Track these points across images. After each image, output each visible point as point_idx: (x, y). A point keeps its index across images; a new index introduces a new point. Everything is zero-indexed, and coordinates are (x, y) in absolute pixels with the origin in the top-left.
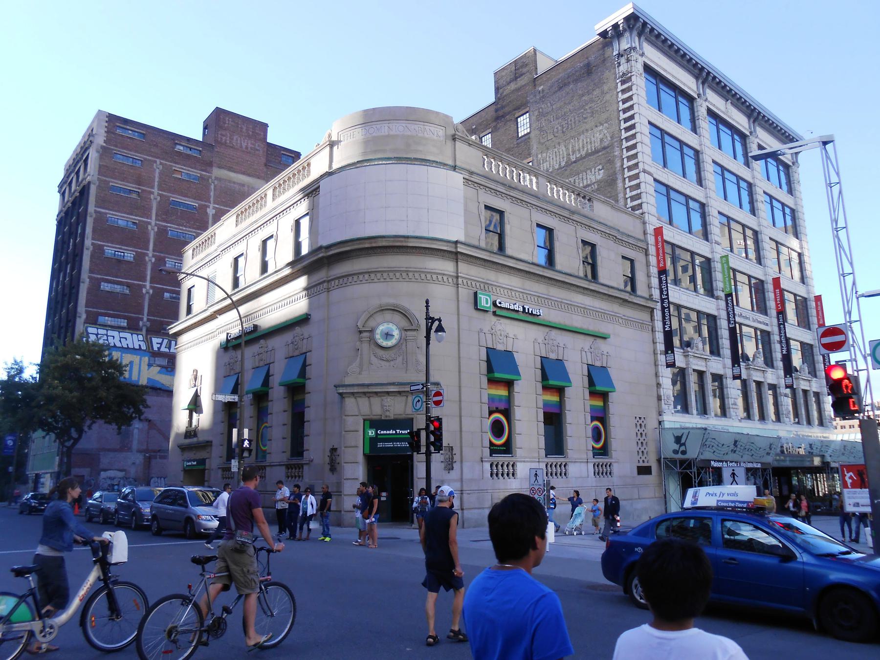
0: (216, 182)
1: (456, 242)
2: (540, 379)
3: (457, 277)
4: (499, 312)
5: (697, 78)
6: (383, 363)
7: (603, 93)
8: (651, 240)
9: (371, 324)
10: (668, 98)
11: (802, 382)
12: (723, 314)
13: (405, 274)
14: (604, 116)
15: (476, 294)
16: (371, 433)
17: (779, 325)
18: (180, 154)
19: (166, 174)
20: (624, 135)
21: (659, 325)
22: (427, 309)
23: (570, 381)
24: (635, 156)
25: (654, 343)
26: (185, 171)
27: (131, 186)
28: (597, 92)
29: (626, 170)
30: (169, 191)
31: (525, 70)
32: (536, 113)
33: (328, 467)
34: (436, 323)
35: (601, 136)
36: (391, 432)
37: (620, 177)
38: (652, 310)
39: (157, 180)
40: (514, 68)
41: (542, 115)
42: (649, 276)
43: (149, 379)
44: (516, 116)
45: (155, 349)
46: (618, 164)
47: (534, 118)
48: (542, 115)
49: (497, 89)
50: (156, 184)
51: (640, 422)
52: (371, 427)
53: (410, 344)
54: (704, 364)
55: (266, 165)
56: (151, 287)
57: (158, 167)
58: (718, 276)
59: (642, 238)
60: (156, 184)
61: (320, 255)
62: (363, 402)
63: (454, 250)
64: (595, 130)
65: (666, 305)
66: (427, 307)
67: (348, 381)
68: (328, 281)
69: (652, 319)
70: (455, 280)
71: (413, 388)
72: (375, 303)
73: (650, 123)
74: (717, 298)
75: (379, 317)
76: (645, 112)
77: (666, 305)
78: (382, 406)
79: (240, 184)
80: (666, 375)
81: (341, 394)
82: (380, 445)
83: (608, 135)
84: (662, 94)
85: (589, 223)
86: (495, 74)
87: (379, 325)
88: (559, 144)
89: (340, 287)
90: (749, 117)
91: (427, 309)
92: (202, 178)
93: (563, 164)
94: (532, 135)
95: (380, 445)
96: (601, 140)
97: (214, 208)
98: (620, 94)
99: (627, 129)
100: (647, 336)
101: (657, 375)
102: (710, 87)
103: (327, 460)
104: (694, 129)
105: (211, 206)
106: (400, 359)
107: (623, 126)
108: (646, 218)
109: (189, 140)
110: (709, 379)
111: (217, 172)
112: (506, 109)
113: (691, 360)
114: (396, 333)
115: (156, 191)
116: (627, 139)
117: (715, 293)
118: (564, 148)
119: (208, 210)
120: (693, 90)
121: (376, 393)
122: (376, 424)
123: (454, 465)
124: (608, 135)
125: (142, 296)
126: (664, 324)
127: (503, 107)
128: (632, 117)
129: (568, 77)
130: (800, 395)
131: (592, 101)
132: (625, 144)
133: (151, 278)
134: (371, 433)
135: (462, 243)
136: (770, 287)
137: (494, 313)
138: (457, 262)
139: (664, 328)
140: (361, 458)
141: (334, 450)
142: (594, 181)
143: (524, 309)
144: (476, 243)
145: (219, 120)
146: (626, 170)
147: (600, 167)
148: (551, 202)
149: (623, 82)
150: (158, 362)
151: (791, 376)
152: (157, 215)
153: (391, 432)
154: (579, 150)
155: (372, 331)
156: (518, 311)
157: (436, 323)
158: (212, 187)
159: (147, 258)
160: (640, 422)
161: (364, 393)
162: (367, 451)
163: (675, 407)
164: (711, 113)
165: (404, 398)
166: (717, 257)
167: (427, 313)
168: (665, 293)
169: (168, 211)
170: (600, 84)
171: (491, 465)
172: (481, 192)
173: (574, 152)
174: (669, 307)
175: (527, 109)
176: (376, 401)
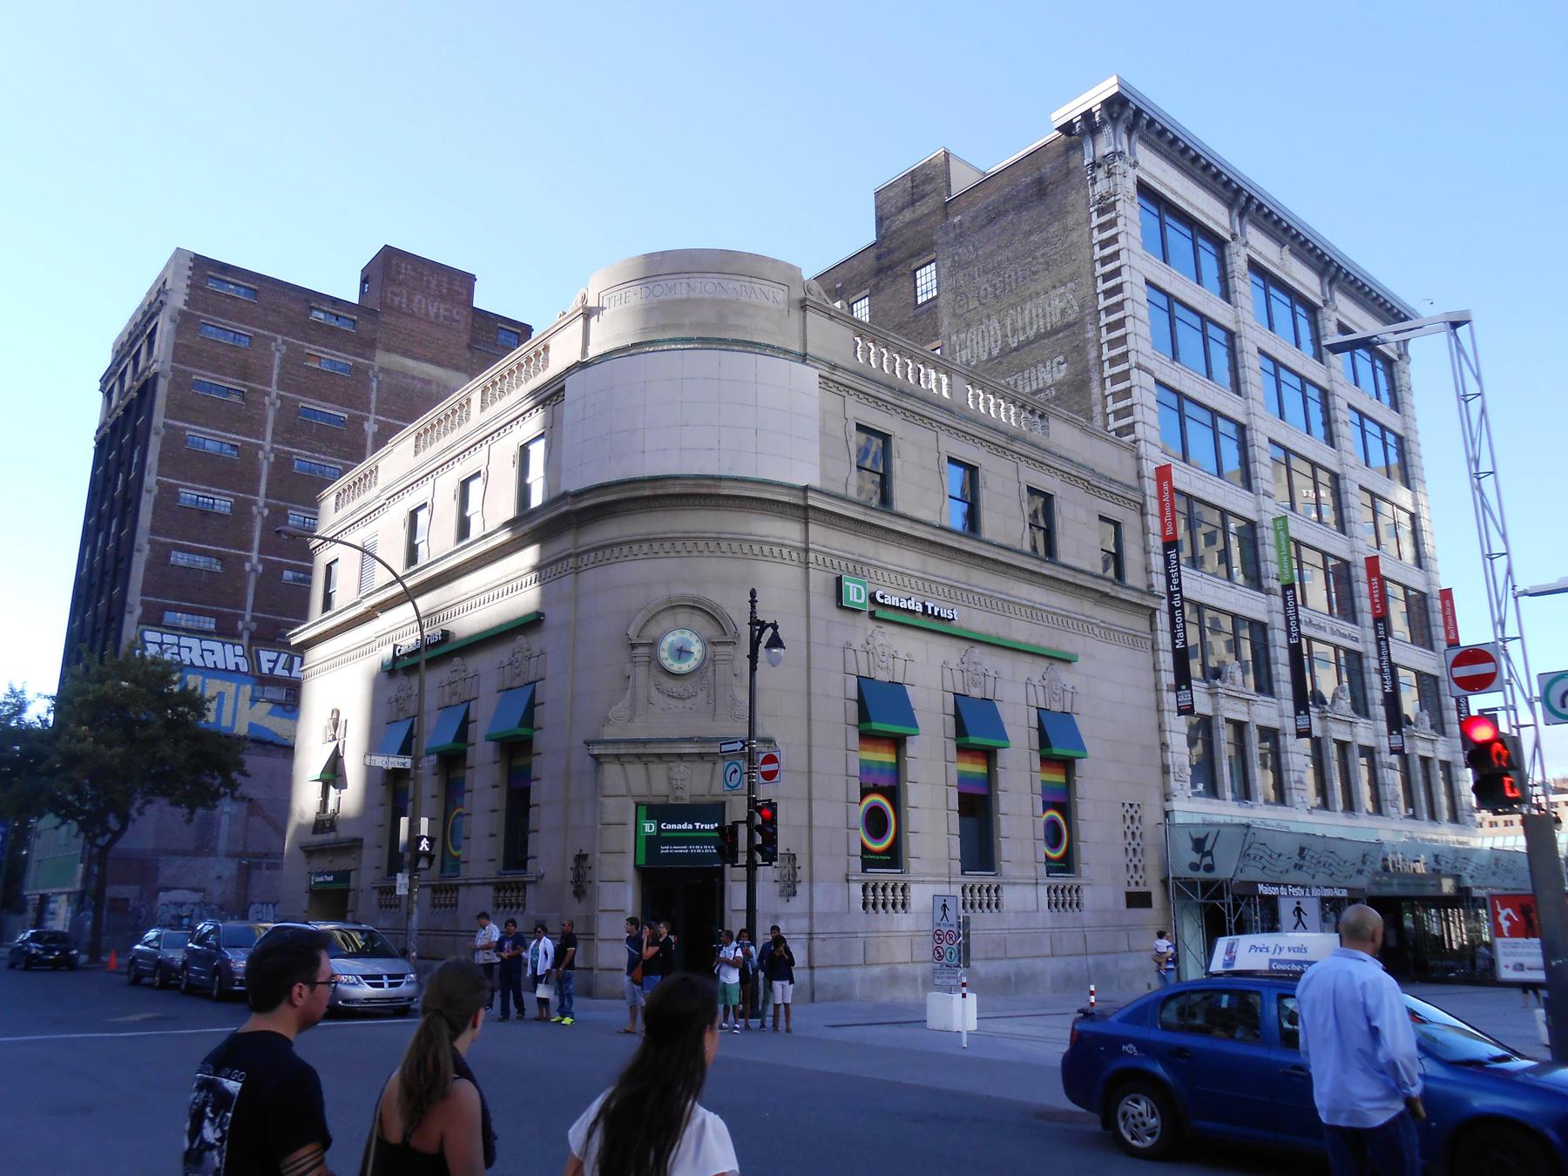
0: (381, 376)
1: (806, 489)
2: (1036, 745)
3: (807, 550)
4: (880, 613)
5: (1230, 206)
6: (672, 702)
7: (1065, 229)
8: (1151, 487)
9: (653, 631)
10: (1179, 240)
11: (1419, 743)
12: (1279, 621)
13: (715, 543)
14: (1068, 270)
15: (839, 580)
16: (649, 828)
17: (1378, 641)
18: (318, 325)
19: (293, 359)
20: (1103, 303)
21: (1164, 639)
22: (753, 607)
23: (1006, 739)
24: (1122, 340)
25: (1156, 670)
26: (326, 357)
27: (229, 382)
28: (1055, 228)
29: (1106, 365)
30: (299, 391)
31: (928, 188)
32: (948, 263)
33: (570, 889)
34: (769, 632)
35: (1063, 305)
36: (685, 826)
37: (1095, 377)
38: (1152, 613)
39: (276, 371)
40: (909, 184)
41: (958, 266)
42: (1146, 552)
43: (251, 725)
44: (914, 266)
45: (265, 670)
46: (1093, 354)
47: (943, 271)
48: (958, 266)
49: (880, 221)
50: (275, 377)
51: (1132, 812)
52: (649, 818)
53: (720, 667)
54: (1245, 709)
55: (469, 347)
56: (261, 560)
57: (279, 347)
58: (1269, 552)
59: (1134, 483)
60: (275, 377)
61: (565, 509)
62: (636, 771)
63: (801, 502)
64: (1052, 293)
65: (1177, 603)
66: (753, 602)
67: (609, 733)
68: (578, 555)
69: (1153, 629)
70: (802, 555)
71: (725, 748)
72: (660, 594)
73: (1148, 282)
74: (1268, 592)
75: (666, 621)
76: (1139, 263)
77: (1177, 603)
78: (670, 779)
79: (423, 380)
80: (1178, 727)
81: (596, 758)
82: (665, 849)
83: (1074, 303)
84: (1170, 232)
85: (1041, 457)
86: (877, 194)
87: (666, 633)
88: (988, 317)
89: (597, 564)
90: (1321, 274)
91: (753, 607)
92: (356, 368)
93: (995, 352)
94: (941, 301)
95: (665, 849)
96: (1063, 311)
97: (377, 422)
98: (1095, 232)
99: (1109, 293)
100: (1144, 658)
101: (1161, 728)
102: (1254, 223)
103: (570, 876)
104: (1226, 295)
105: (372, 417)
106: (702, 696)
107: (1101, 287)
108: (1142, 450)
109: (335, 301)
110: (1253, 737)
111: (382, 359)
112: (896, 256)
113: (1222, 701)
114: (696, 648)
115: (274, 390)
116: (1109, 310)
117: (1264, 582)
118: (997, 326)
119: (366, 425)
120: (1223, 227)
121: (660, 756)
122: (658, 811)
123: (798, 888)
124: (1074, 303)
125: (244, 576)
126: (1174, 637)
127: (890, 252)
128: (1117, 272)
129: (1006, 201)
130: (1417, 766)
131: (1046, 242)
132: (1104, 320)
133: (261, 545)
134: (649, 828)
135: (815, 490)
136: (1360, 573)
137: (872, 615)
138: (806, 524)
139: (1174, 644)
140: (630, 873)
141: (581, 858)
142: (1050, 382)
143: (925, 607)
144: (841, 491)
145: (390, 268)
146: (1106, 365)
147: (1061, 359)
148: (974, 419)
149: (1101, 212)
150: (268, 695)
151: (1400, 733)
152: (274, 433)
153: (685, 826)
154: (1024, 329)
155: (654, 645)
156: (914, 612)
157: (769, 632)
158: (374, 385)
159: (254, 509)
160: (1132, 812)
161: (638, 756)
162: (642, 861)
163: (1194, 786)
164: (1254, 267)
165: (710, 765)
166: (1267, 519)
167: (753, 612)
168: (1175, 582)
169: (295, 426)
170: (1060, 214)
171: (864, 889)
172: (851, 400)
173: (1014, 332)
174: (1182, 607)
175: (933, 256)
176: (659, 770)
